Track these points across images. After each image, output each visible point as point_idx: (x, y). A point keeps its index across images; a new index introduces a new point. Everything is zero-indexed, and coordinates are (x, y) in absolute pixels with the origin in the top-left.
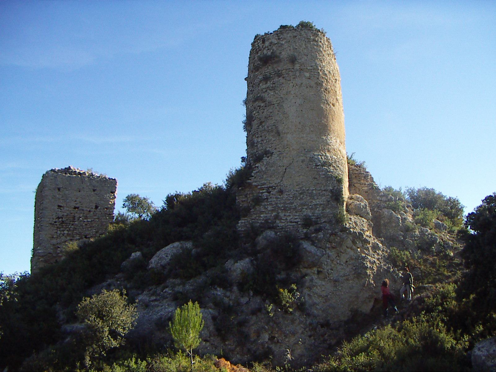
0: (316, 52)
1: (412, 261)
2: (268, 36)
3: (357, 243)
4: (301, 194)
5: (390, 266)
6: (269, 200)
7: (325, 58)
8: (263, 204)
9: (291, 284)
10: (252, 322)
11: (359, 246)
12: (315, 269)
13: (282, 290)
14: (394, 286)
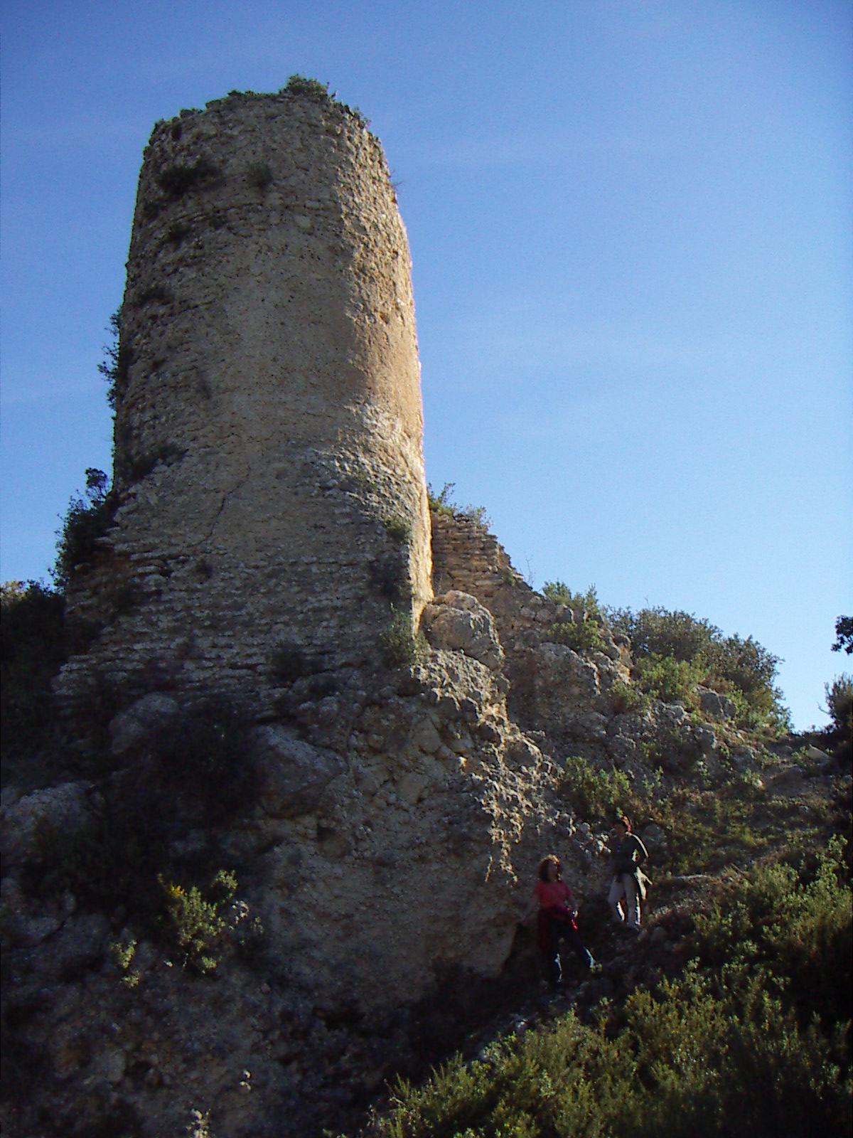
0: (333, 163)
1: (636, 802)
2: (190, 117)
3: (455, 738)
4: (270, 576)
5: (566, 815)
6: (165, 597)
7: (362, 185)
8: (144, 609)
9: (215, 871)
10: (63, 1009)
11: (462, 749)
12: (309, 821)
13: (177, 891)
14: (580, 884)
